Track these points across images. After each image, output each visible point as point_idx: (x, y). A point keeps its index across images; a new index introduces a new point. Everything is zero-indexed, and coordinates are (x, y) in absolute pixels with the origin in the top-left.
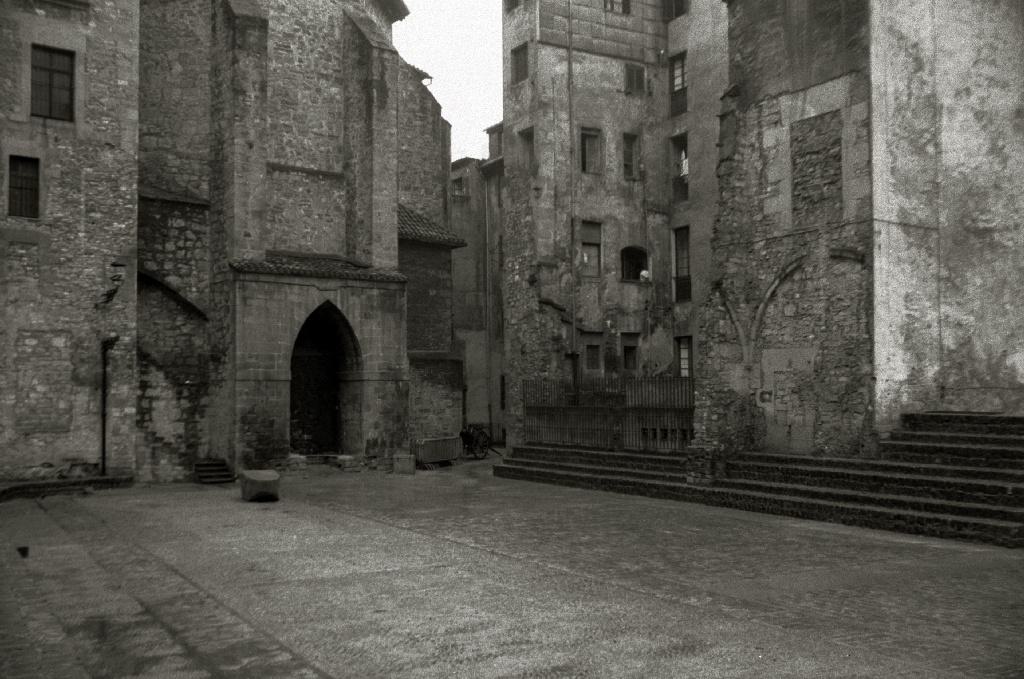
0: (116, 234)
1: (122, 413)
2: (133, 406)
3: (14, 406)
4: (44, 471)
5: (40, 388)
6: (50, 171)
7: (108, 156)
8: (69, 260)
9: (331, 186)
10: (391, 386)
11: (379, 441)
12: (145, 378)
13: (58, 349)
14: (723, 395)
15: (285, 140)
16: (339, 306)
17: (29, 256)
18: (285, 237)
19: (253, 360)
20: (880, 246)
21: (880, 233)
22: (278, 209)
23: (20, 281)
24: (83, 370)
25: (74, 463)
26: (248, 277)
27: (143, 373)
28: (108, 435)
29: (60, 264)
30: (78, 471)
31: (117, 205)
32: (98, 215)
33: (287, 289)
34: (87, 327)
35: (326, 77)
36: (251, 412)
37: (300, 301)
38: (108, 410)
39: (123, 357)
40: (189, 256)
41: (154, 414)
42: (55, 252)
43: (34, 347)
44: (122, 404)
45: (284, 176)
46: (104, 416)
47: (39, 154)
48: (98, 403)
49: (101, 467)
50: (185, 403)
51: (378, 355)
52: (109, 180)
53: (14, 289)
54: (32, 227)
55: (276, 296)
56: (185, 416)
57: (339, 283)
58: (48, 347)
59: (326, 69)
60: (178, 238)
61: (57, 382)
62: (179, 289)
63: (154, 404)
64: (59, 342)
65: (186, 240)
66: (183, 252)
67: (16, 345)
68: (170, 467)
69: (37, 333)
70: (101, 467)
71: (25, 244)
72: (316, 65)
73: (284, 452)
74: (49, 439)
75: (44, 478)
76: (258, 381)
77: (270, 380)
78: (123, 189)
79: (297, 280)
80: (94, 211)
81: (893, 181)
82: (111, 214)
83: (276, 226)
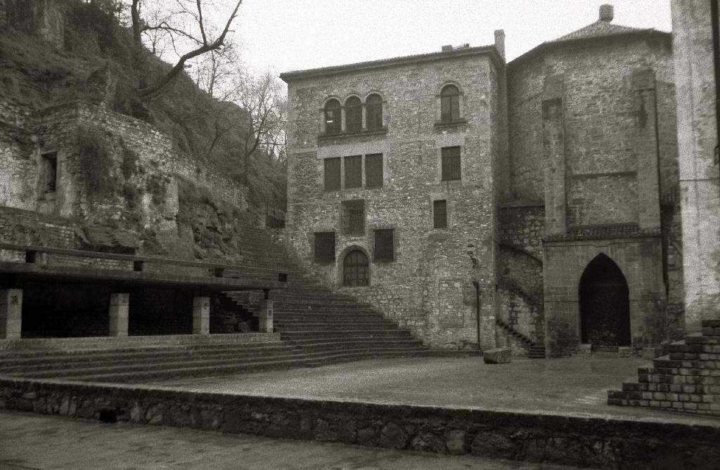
0: (482, 230)
1: (488, 319)
2: (493, 315)
3: (439, 315)
4: (452, 346)
5: (450, 307)
6: (451, 204)
7: (476, 192)
8: (460, 245)
9: (627, 180)
10: (651, 304)
11: (643, 339)
12: (513, 301)
13: (457, 288)
14: (674, 307)
15: (596, 159)
16: (610, 256)
17: (444, 245)
18: (596, 217)
19: (554, 291)
20: (687, 199)
21: (687, 189)
22: (591, 200)
23: (439, 258)
24: (468, 298)
25: (465, 343)
26: (549, 245)
27: (512, 299)
28: (481, 330)
29: (457, 248)
30: (468, 347)
31: (482, 215)
32: (473, 222)
33: (574, 248)
34: (469, 276)
35: (622, 114)
36: (554, 319)
37: (584, 254)
38: (481, 317)
39: (487, 291)
40: (537, 234)
41: (518, 320)
42: (454, 242)
43: (447, 288)
44: (488, 314)
45: (594, 180)
46: (478, 320)
47: (446, 198)
48: (476, 314)
49: (478, 345)
50: (535, 314)
51: (640, 285)
52: (477, 204)
53: (437, 261)
54: (444, 232)
55: (567, 253)
56: (535, 322)
57: (609, 242)
58: (452, 287)
59: (622, 109)
60: (531, 226)
61: (457, 304)
62: (533, 253)
63: (519, 315)
64: (457, 285)
65: (536, 226)
66: (534, 233)
67: (439, 288)
68: (516, 348)
69: (447, 281)
70: (478, 345)
71: (441, 241)
72: (615, 110)
73: (576, 343)
74: (454, 331)
75: (452, 349)
76: (558, 303)
77: (565, 301)
78: (485, 207)
79: (580, 243)
80: (471, 220)
81: (701, 150)
82: (479, 221)
83: (590, 211)
